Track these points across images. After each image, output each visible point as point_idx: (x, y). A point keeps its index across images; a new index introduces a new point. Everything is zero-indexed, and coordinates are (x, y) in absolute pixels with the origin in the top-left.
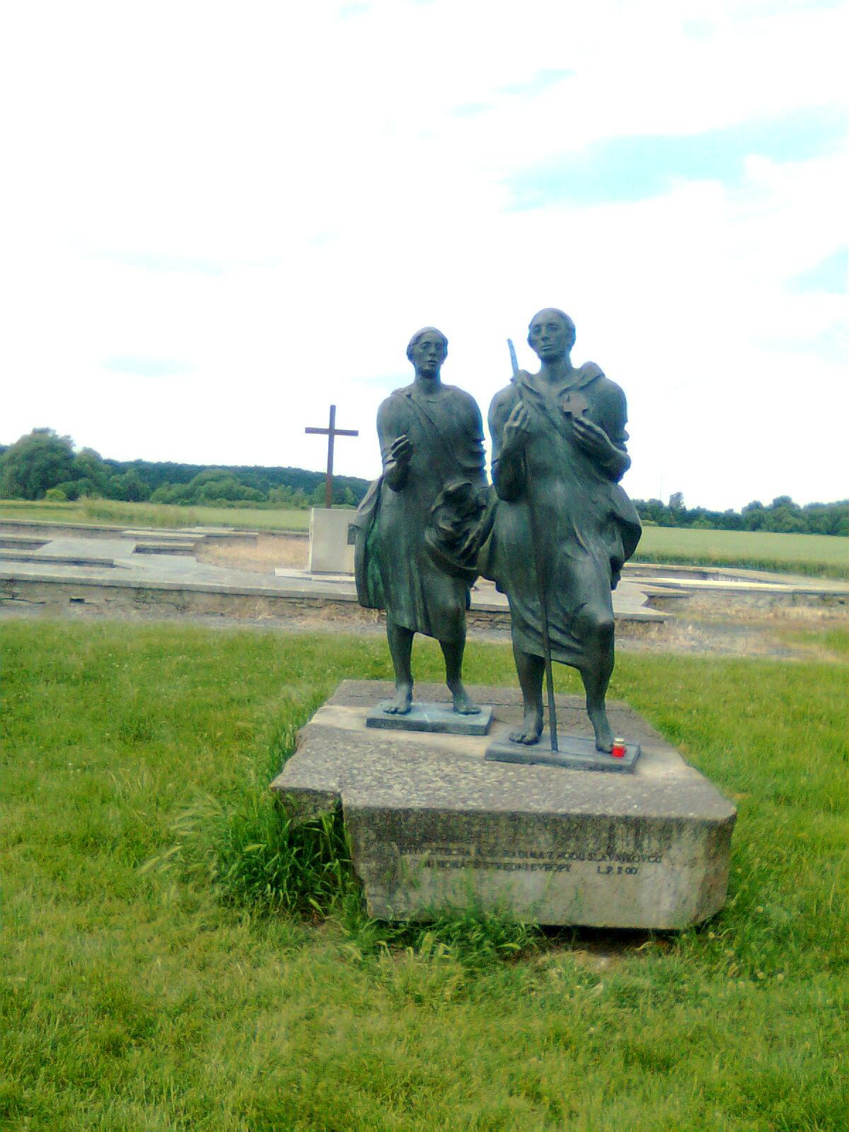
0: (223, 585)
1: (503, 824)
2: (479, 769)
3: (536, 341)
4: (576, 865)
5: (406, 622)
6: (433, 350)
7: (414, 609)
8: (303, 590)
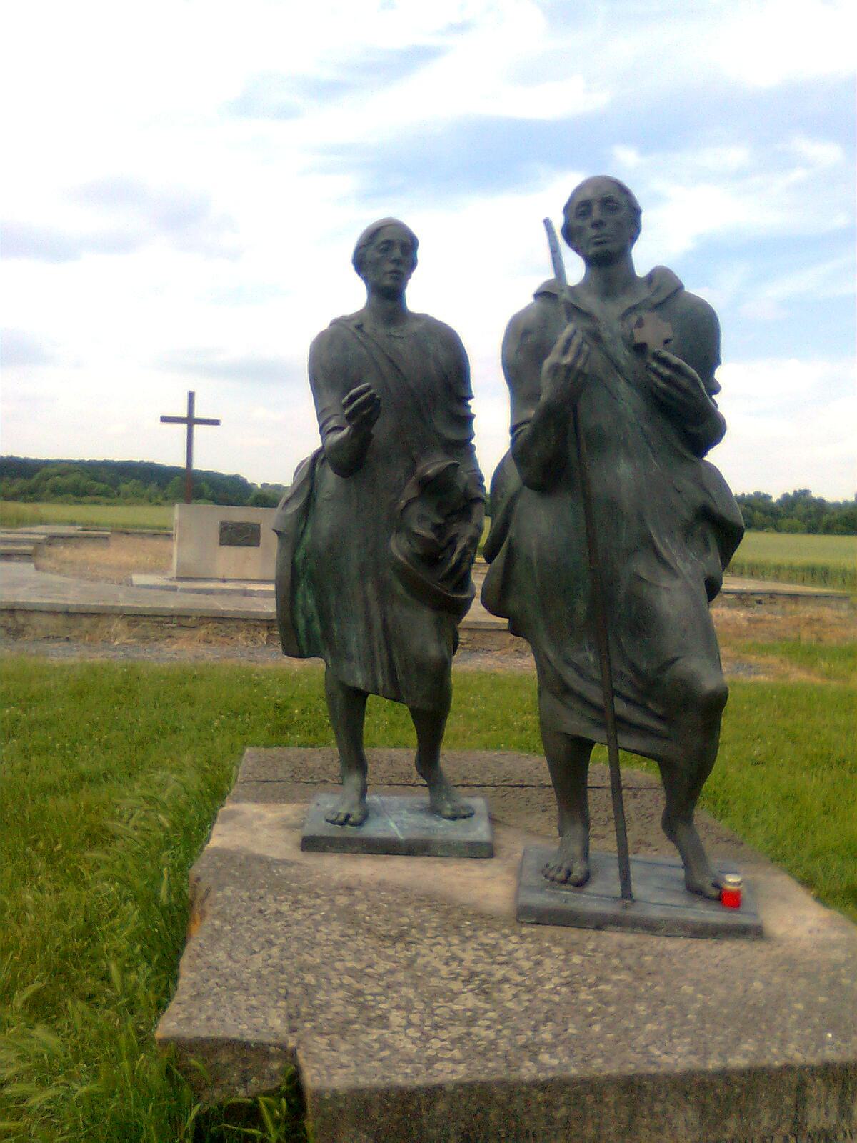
0: (69, 602)
1: (610, 1100)
3: (580, 230)
5: (359, 680)
6: (397, 253)
7: (373, 662)
8: (172, 606)
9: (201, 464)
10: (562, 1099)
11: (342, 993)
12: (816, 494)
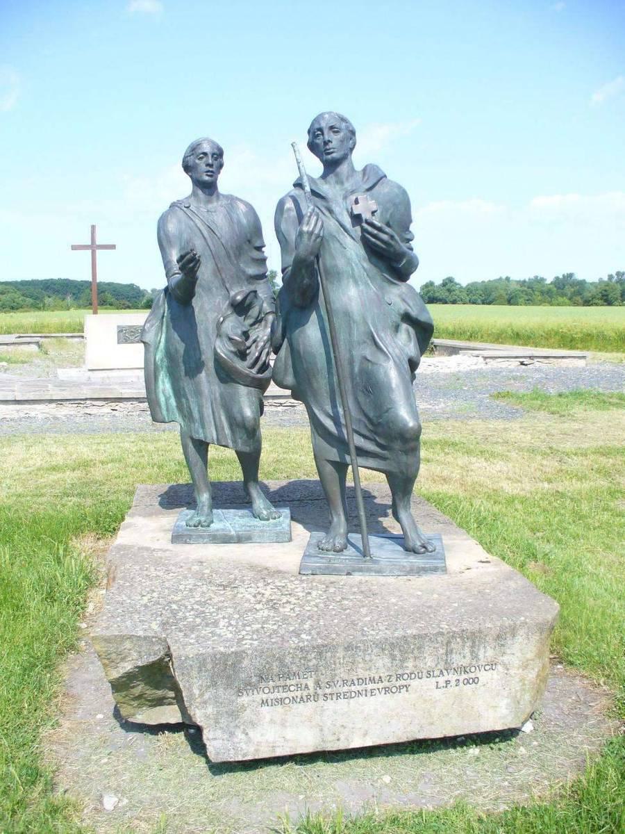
2: (299, 588)
4: (415, 683)
9: (104, 277)
10: (313, 655)
11: (192, 613)
12: (579, 276)
